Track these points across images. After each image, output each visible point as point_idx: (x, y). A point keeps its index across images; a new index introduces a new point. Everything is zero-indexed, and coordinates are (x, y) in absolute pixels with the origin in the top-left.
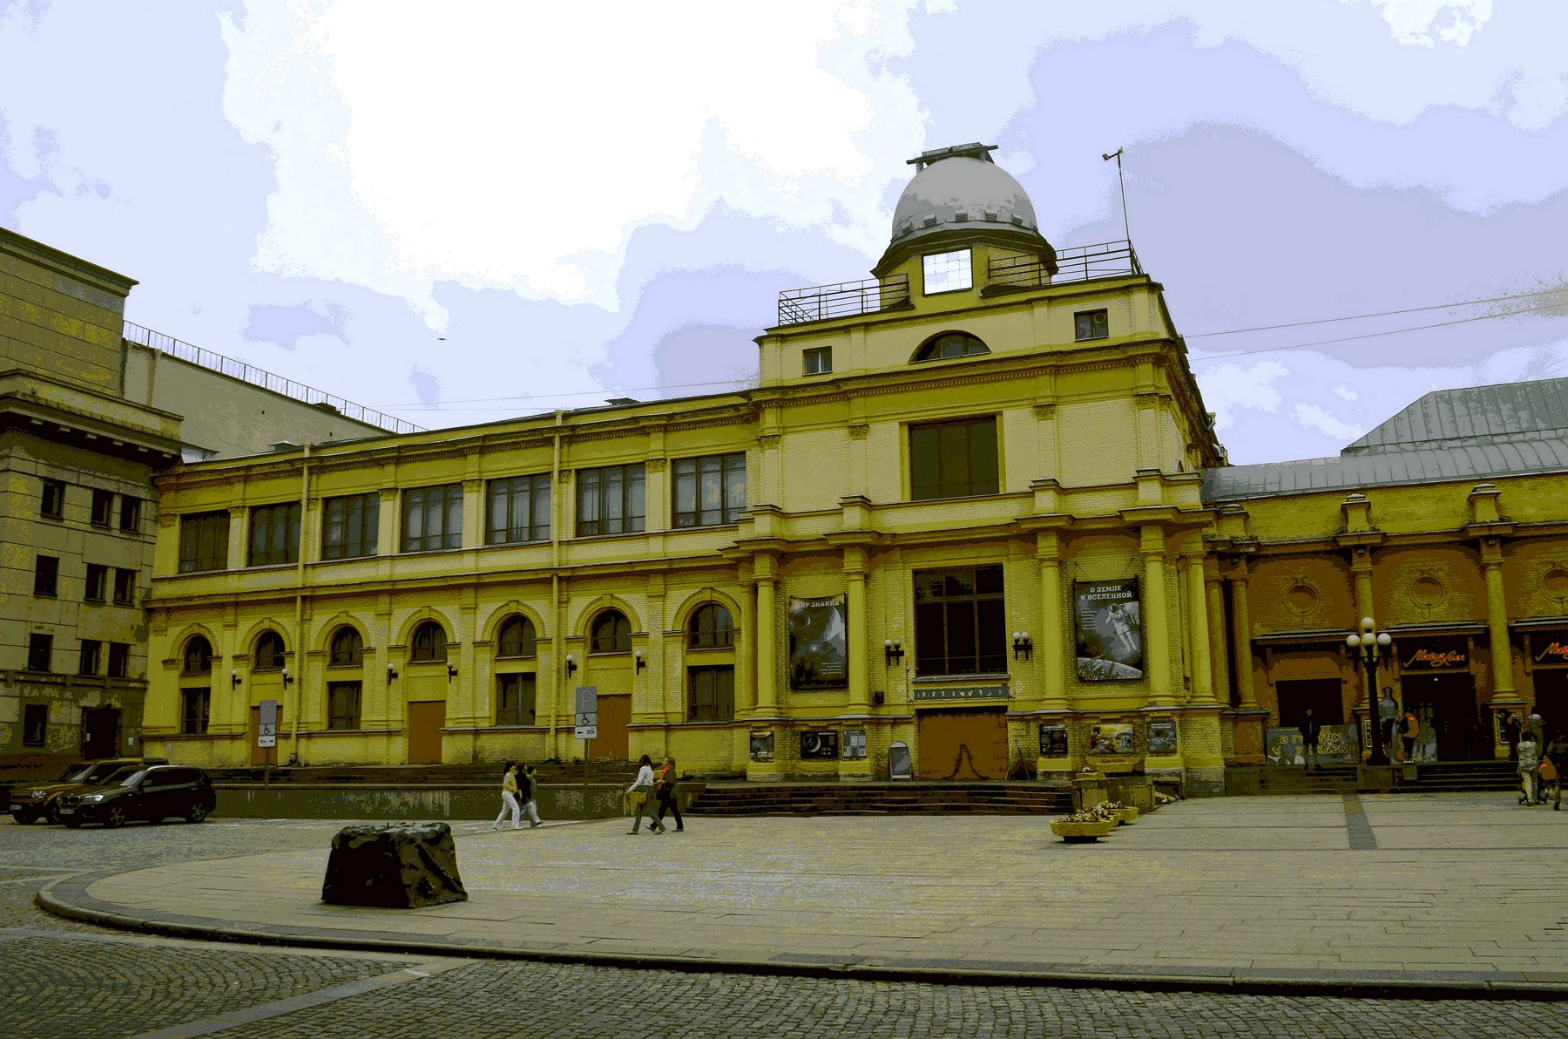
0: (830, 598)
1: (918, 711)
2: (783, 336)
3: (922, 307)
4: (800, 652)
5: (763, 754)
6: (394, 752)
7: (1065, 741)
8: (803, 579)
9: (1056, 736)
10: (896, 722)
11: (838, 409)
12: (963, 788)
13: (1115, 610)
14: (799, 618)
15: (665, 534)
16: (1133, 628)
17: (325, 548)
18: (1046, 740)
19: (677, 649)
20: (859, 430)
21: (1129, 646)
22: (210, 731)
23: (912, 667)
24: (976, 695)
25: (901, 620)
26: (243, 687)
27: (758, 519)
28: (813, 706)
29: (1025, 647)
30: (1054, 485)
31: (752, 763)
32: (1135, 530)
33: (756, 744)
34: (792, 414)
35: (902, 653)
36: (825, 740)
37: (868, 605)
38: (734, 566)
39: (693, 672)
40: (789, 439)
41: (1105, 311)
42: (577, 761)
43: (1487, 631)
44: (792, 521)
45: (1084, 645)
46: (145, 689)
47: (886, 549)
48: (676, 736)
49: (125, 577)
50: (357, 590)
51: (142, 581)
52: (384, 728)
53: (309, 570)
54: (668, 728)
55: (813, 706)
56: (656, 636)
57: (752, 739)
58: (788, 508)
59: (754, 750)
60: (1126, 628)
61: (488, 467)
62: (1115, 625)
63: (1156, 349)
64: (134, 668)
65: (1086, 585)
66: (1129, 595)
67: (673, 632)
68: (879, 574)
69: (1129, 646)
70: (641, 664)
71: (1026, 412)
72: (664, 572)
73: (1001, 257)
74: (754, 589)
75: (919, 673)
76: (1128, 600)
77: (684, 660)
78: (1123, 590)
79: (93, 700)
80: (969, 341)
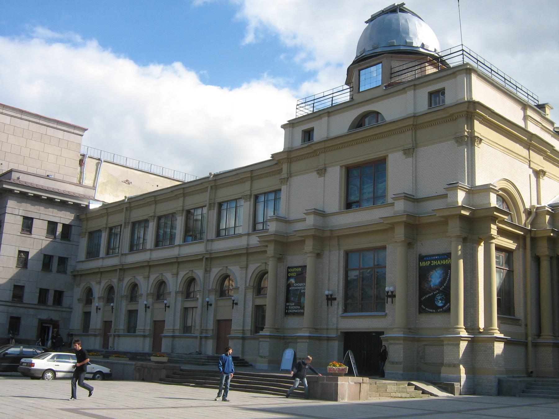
2: (415, 85)
20: (322, 172)
22: (90, 332)
42: (440, 373)
46: (71, 312)
49: (63, 261)
50: (229, 254)
51: (71, 264)
58: (292, 217)
63: (410, 122)
64: (66, 301)
73: (397, 64)
77: (253, 302)
79: (45, 315)
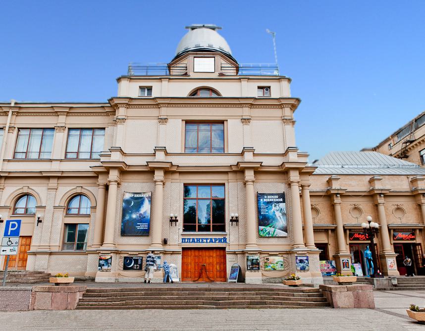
1: (183, 249)
3: (192, 75)
4: (127, 218)
5: (105, 267)
7: (258, 264)
9: (254, 261)
10: (173, 253)
11: (154, 112)
14: (127, 202)
15: (61, 161)
16: (284, 214)
18: (249, 263)
19: (60, 214)
20: (163, 120)
21: (281, 222)
23: (181, 228)
24: (211, 241)
25: (178, 206)
27: (113, 154)
28: (133, 245)
29: (235, 220)
30: (251, 150)
31: (99, 272)
33: (102, 262)
34: (132, 112)
35: (177, 221)
37: (164, 197)
38: (96, 176)
40: (129, 122)
41: (269, 87)
43: (336, 228)
44: (128, 157)
45: (264, 220)
47: (174, 172)
55: (133, 245)
56: (50, 207)
57: (100, 259)
59: (100, 265)
60: (280, 214)
62: (276, 211)
65: (262, 195)
66: (281, 200)
68: (168, 184)
69: (281, 222)
70: (39, 221)
71: (238, 122)
72: (59, 178)
74: (107, 187)
75: (184, 230)
76: (281, 202)
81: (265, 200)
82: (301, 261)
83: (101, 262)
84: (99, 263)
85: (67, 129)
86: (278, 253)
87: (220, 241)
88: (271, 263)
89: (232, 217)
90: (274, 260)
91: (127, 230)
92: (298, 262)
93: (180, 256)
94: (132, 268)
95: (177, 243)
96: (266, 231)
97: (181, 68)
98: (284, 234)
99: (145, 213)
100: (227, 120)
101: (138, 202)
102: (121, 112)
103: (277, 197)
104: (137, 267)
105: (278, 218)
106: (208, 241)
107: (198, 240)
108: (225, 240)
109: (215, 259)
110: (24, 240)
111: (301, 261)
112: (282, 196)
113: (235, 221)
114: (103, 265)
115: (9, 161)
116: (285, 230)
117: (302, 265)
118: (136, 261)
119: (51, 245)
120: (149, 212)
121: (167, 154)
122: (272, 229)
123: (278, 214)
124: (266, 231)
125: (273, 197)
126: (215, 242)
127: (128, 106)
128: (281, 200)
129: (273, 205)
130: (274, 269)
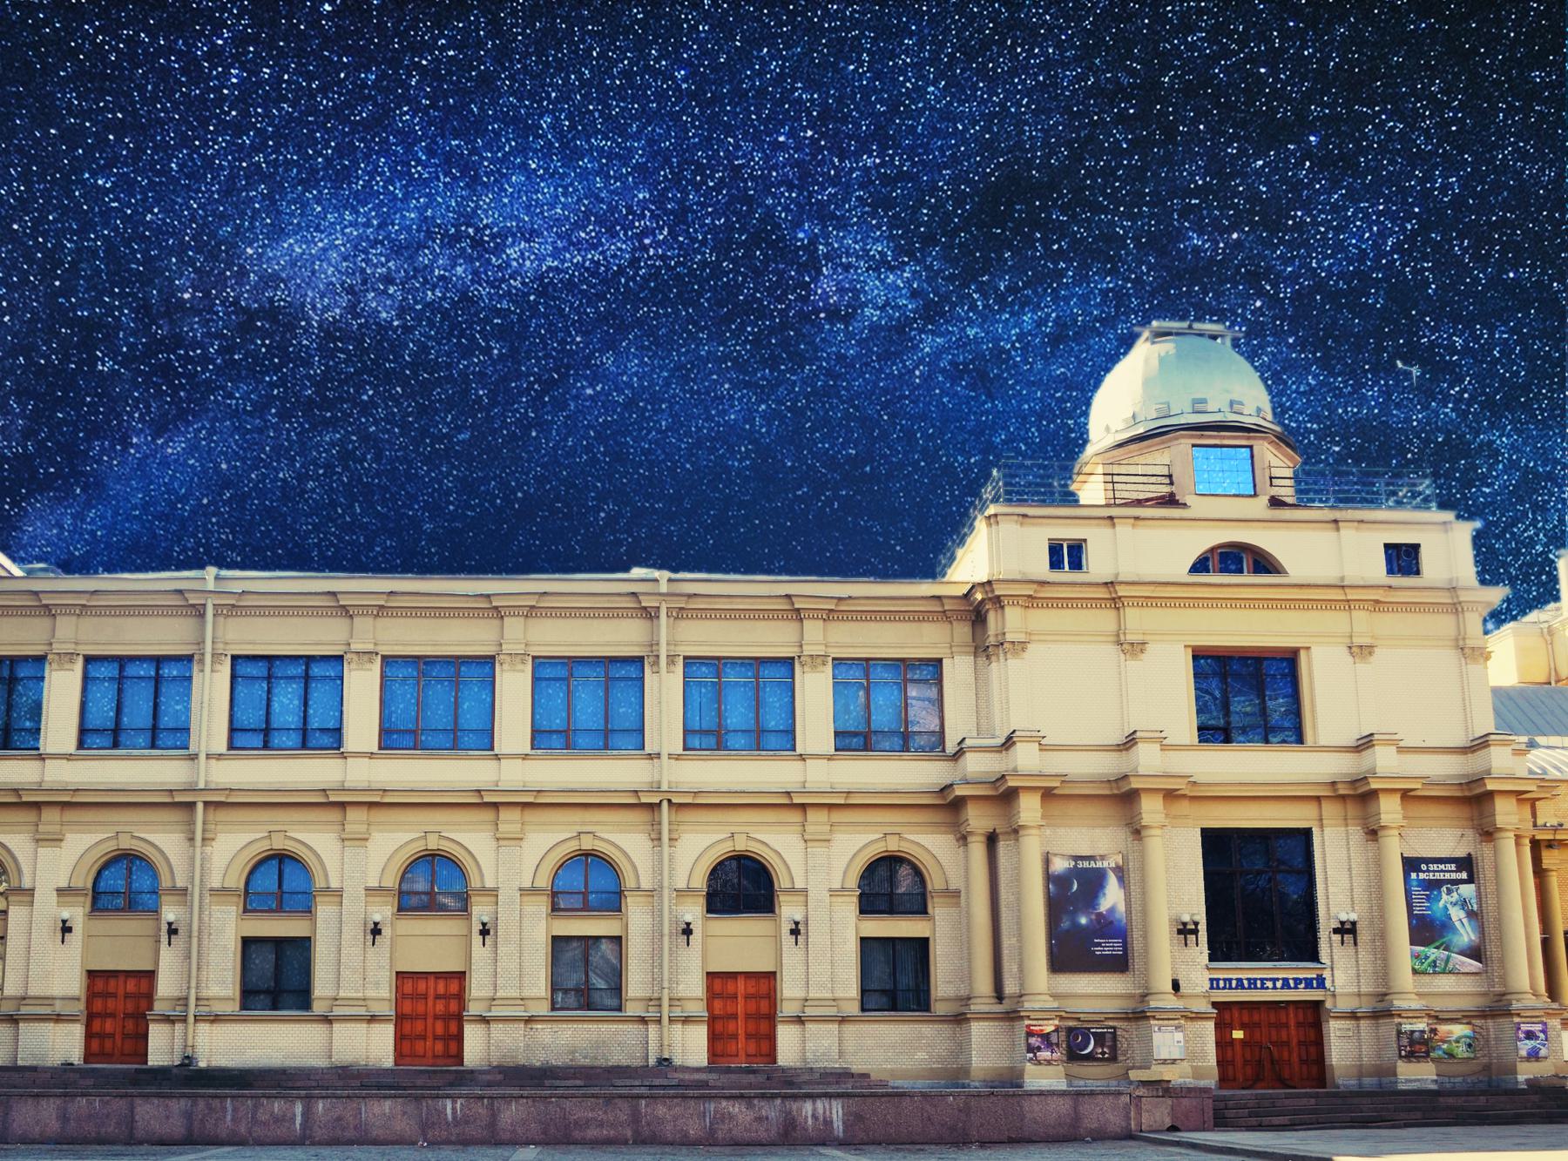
0: (1103, 858)
6: (375, 1046)
8: (1061, 831)
12: (298, 1088)
13: (1449, 892)
16: (1471, 915)
17: (84, 732)
20: (1135, 648)
26: (76, 938)
29: (1347, 930)
32: (957, 805)
34: (1041, 619)
36: (1100, 1039)
39: (558, 942)
45: (1426, 930)
48: (849, 1029)
52: (832, 1011)
53: (213, 762)
54: (843, 1020)
57: (1030, 1034)
59: (1030, 1049)
60: (1462, 914)
61: (230, 636)
62: (1449, 904)
67: (380, 889)
69: (1466, 934)
78: (1458, 870)
80: (1264, 564)
81: (1422, 876)
82: (1530, 1035)
83: (1033, 1040)
84: (1029, 1045)
85: (80, 660)
86: (1459, 1015)
87: (1308, 983)
88: (1444, 1042)
89: (1342, 923)
90: (1450, 1032)
91: (1070, 953)
92: (1522, 1036)
93: (1211, 1025)
94: (1090, 1057)
95: (1199, 990)
96: (1427, 958)
97: (1153, 480)
98: (1473, 965)
99: (1112, 910)
100: (1308, 648)
101: (1089, 881)
102: (1013, 622)
103: (1453, 867)
104: (1103, 1053)
105: (1458, 924)
106: (1279, 984)
107: (1252, 982)
108: (1321, 982)
109: (1293, 1032)
110: (752, 982)
111: (1530, 1035)
112: (1466, 864)
113: (1348, 931)
114: (1039, 1049)
115: (220, 757)
116: (1475, 953)
117: (1530, 1044)
118: (1100, 1039)
119: (526, 994)
120: (1121, 908)
121: (1043, 748)
122: (1443, 954)
123: (1457, 914)
124: (1427, 958)
125: (1442, 867)
126: (1296, 987)
127: (1031, 601)
128: (1464, 875)
129: (1444, 889)
130: (1451, 1055)
